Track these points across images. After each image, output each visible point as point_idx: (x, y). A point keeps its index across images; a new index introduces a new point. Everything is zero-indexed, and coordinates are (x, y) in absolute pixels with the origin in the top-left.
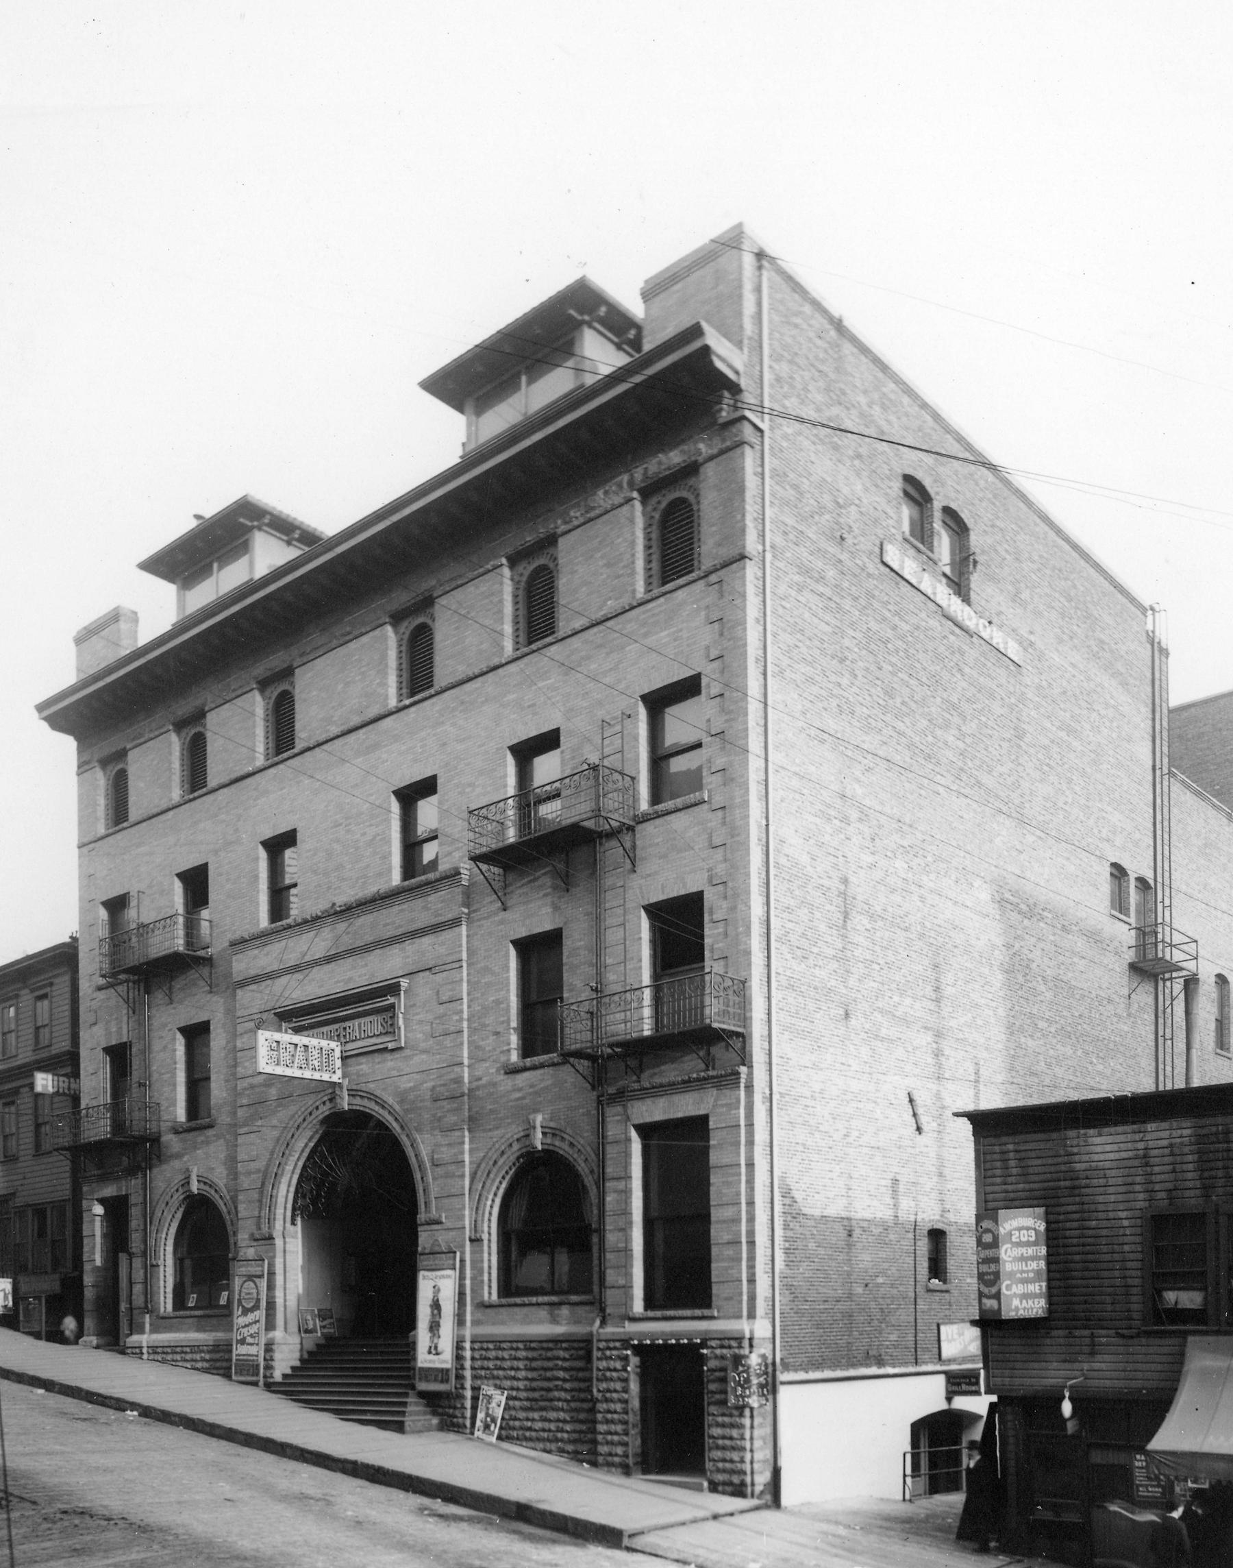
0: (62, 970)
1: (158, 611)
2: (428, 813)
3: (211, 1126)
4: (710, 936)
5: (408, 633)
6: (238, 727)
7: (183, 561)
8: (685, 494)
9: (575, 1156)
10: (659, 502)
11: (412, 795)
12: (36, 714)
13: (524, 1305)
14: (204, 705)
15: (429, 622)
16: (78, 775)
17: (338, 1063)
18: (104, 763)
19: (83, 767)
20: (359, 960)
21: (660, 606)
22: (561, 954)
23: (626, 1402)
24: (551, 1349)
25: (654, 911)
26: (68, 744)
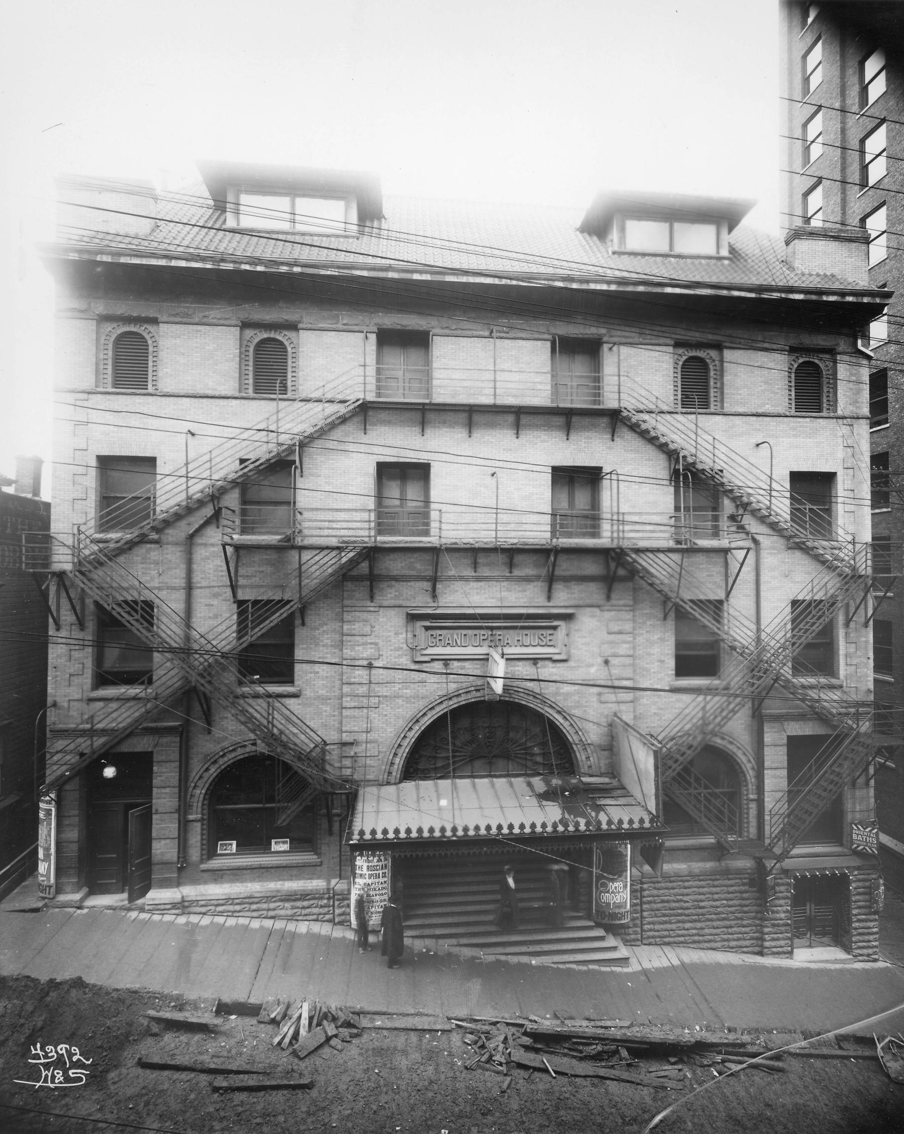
3: (295, 696)
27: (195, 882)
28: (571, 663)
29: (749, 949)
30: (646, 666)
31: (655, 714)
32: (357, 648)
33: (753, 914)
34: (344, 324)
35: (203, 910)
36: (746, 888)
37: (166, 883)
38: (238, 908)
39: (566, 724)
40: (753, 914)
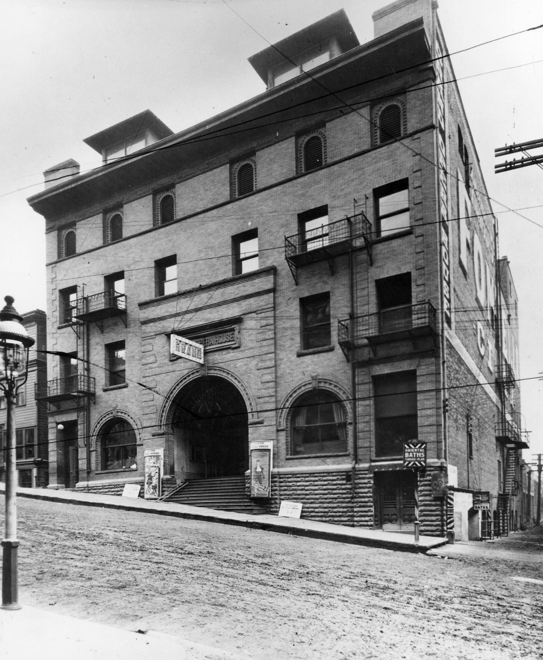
0: (34, 323)
1: (91, 161)
2: (120, 286)
3: (126, 387)
4: (414, 292)
5: (239, 168)
6: (138, 213)
8: (119, 213)
9: (338, 391)
10: (381, 107)
13: (309, 458)
14: (123, 201)
15: (74, 231)
16: (46, 234)
17: (202, 355)
18: (60, 229)
19: (49, 230)
20: (214, 310)
21: (384, 150)
22: (329, 302)
24: (308, 477)
25: (381, 284)
26: (40, 220)
27: (93, 479)
28: (242, 349)
29: (347, 523)
30: (283, 344)
31: (289, 373)
32: (147, 358)
33: (349, 500)
34: (140, 195)
35: (95, 491)
36: (344, 482)
37: (83, 480)
38: (107, 490)
39: (239, 385)
40: (349, 500)
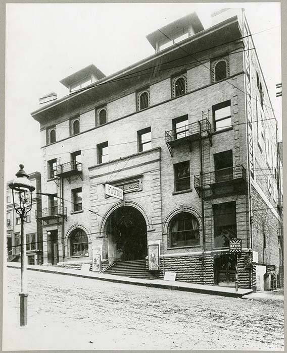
1: (63, 93)
3: (82, 212)
6: (88, 119)
7: (69, 82)
11: (175, 121)
12: (31, 116)
19: (42, 129)
23: (275, 288)
25: (215, 155)
26: (37, 124)
